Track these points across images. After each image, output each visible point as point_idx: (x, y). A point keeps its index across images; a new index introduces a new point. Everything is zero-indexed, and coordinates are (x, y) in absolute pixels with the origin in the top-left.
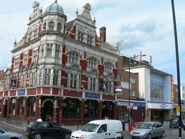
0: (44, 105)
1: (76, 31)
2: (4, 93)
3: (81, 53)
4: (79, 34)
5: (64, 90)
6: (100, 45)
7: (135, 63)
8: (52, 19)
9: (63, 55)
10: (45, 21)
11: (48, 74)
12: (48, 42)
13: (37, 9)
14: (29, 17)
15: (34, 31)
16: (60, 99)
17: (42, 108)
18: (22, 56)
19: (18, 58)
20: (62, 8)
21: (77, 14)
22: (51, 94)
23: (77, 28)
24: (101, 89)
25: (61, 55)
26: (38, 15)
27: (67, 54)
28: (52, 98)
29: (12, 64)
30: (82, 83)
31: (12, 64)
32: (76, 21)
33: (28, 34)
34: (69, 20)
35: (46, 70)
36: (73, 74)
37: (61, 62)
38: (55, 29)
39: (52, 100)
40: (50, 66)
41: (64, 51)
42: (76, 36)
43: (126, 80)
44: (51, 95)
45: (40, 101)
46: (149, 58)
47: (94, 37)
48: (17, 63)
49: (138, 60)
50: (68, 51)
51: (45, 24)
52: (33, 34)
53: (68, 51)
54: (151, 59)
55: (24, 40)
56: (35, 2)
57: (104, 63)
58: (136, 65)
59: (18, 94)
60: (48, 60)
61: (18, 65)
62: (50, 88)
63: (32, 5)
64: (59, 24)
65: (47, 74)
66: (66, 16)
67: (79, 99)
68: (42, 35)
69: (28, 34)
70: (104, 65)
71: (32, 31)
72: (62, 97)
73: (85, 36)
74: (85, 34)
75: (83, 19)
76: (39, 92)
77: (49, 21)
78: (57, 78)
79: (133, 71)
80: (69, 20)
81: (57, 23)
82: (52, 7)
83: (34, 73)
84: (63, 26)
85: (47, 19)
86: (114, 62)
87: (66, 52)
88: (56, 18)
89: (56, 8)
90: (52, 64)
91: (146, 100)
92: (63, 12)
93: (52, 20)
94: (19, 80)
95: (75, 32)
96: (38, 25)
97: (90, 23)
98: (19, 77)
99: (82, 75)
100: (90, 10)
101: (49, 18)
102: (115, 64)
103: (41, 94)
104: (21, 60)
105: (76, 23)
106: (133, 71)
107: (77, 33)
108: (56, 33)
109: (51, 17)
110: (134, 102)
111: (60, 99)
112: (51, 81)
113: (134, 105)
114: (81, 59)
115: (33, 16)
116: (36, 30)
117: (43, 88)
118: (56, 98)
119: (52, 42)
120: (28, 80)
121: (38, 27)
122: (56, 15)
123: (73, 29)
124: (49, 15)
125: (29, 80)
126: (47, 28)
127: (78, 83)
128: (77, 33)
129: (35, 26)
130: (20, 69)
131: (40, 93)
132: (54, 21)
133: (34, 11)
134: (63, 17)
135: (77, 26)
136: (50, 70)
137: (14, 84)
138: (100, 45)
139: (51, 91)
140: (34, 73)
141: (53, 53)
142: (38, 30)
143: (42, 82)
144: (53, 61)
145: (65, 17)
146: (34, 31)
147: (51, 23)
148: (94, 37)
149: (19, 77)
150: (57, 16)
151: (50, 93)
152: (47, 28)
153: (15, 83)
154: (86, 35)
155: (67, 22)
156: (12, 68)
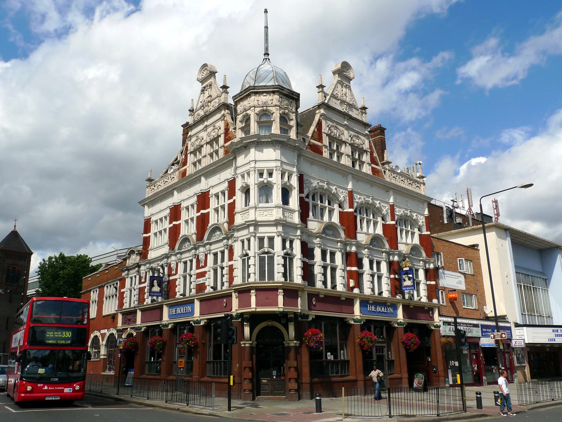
0: (256, 341)
1: (324, 136)
2: (120, 317)
5: (309, 294)
7: (459, 220)
8: (265, 104)
9: (301, 200)
10: (245, 110)
11: (267, 253)
12: (259, 165)
13: (211, 85)
14: (189, 108)
15: (207, 143)
16: (300, 319)
17: (251, 348)
18: (175, 213)
19: (161, 220)
20: (286, 75)
21: (322, 91)
22: (280, 305)
23: (325, 129)
24: (397, 288)
25: (294, 202)
26: (217, 100)
27: (307, 196)
28: (282, 317)
30: (350, 275)
32: (322, 111)
33: (191, 153)
34: (305, 105)
35: (261, 239)
37: (296, 219)
38: (276, 129)
39: (280, 322)
40: (273, 229)
41: (301, 190)
42: (324, 150)
43: (450, 265)
44: (281, 310)
45: (247, 330)
46: (491, 204)
49: (464, 213)
50: (311, 190)
51: (247, 119)
52: (207, 149)
53: (311, 190)
54: (497, 207)
55: (179, 169)
56: (205, 65)
58: (460, 226)
59: (170, 316)
60: (266, 213)
61: (166, 238)
62: (275, 289)
63: (195, 73)
64: (284, 119)
65: (265, 253)
66: (298, 95)
67: (346, 318)
68: (241, 147)
69: (191, 153)
71: (202, 143)
72: (306, 313)
74: (345, 143)
75: (335, 104)
76: (244, 303)
77: (258, 110)
78: (291, 260)
79: (466, 240)
80: (305, 105)
81: (278, 115)
82: (261, 72)
83: (134, 278)
84: (293, 123)
85: (252, 104)
88: (275, 102)
89: (271, 75)
90: (276, 223)
91: (510, 319)
92: (290, 85)
93: (265, 108)
95: (320, 139)
96: (221, 124)
97: (354, 114)
98: (170, 269)
100: (349, 79)
101: (256, 103)
103: (253, 306)
105: (321, 116)
106: (466, 240)
107: (326, 140)
108: (280, 141)
109: (263, 98)
110: (483, 326)
111: (300, 319)
112: (278, 269)
113: (482, 335)
114: (341, 210)
115: (200, 104)
116: (216, 139)
117: (258, 289)
118: (292, 316)
119: (272, 165)
120: (202, 275)
121: (222, 131)
122: (274, 92)
124: (256, 93)
125: (205, 272)
126: (254, 128)
127: (339, 273)
128: (326, 140)
129: (209, 130)
130: (172, 245)
131: (249, 305)
132: (273, 109)
133: (203, 91)
134: (293, 98)
135: (324, 122)
136: (271, 239)
138: (383, 170)
139: (281, 298)
140: (134, 278)
141: (277, 195)
142: (221, 140)
143: (252, 275)
144: (277, 214)
145: (294, 97)
146: (207, 143)
147: (264, 114)
148: (366, 151)
149: (170, 269)
150: (276, 97)
151: (276, 304)
152: (254, 128)
153: (159, 285)
154: (348, 145)
155: (300, 110)
156: (143, 248)
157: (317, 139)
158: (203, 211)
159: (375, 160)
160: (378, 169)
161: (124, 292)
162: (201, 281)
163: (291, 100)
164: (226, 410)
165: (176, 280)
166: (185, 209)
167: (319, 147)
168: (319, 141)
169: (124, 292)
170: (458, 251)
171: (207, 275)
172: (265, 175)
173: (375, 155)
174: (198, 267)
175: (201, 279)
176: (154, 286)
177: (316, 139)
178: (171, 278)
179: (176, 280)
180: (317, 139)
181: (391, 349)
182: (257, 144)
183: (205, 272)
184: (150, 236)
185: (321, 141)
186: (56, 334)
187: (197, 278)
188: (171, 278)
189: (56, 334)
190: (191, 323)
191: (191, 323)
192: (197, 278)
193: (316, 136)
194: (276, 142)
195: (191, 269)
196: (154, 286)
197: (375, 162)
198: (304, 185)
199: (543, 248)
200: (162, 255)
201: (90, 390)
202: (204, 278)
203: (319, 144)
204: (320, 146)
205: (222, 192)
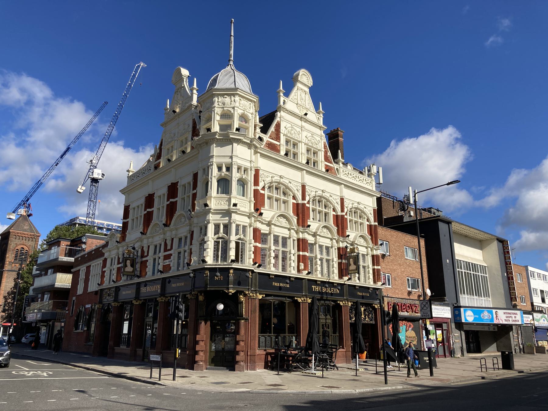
1: (282, 135)
3: (294, 189)
4: (287, 142)
6: (336, 167)
9: (256, 192)
19: (138, 207)
27: (263, 188)
29: (125, 221)
31: (125, 221)
36: (278, 236)
41: (256, 183)
43: (398, 252)
47: (321, 151)
48: (137, 218)
57: (346, 210)
70: (346, 214)
73: (302, 149)
79: (38, 272)
86: (369, 208)
87: (261, 184)
94: (143, 256)
95: (278, 138)
99: (298, 240)
102: (372, 213)
104: (171, 200)
106: (38, 272)
114: (295, 201)
120: (167, 257)
123: (274, 130)
125: (171, 255)
128: (283, 139)
137: (129, 269)
138: (336, 167)
157: (275, 138)
158: (171, 200)
159: (329, 159)
160: (331, 167)
161: (105, 271)
162: (167, 262)
163: (250, 103)
164: (419, 323)
165: (147, 261)
166: (157, 197)
167: (276, 145)
168: (276, 141)
169: (105, 271)
170: (404, 240)
171: (172, 257)
172: (224, 169)
173: (329, 154)
174: (166, 250)
175: (167, 261)
176: (127, 266)
177: (274, 139)
178: (144, 259)
179: (147, 261)
180: (275, 138)
181: (154, 355)
182: (217, 141)
183: (171, 255)
184: (128, 221)
185: (278, 140)
186: (173, 299)
187: (164, 259)
188: (144, 259)
189: (173, 299)
190: (187, 296)
191: (187, 296)
192: (164, 259)
193: (274, 136)
194: (234, 140)
195: (160, 252)
196: (127, 266)
197: (329, 160)
198: (260, 178)
199: (484, 239)
200: (136, 239)
201: (320, 318)
202: (169, 260)
203: (278, 143)
204: (277, 145)
205: (188, 183)
